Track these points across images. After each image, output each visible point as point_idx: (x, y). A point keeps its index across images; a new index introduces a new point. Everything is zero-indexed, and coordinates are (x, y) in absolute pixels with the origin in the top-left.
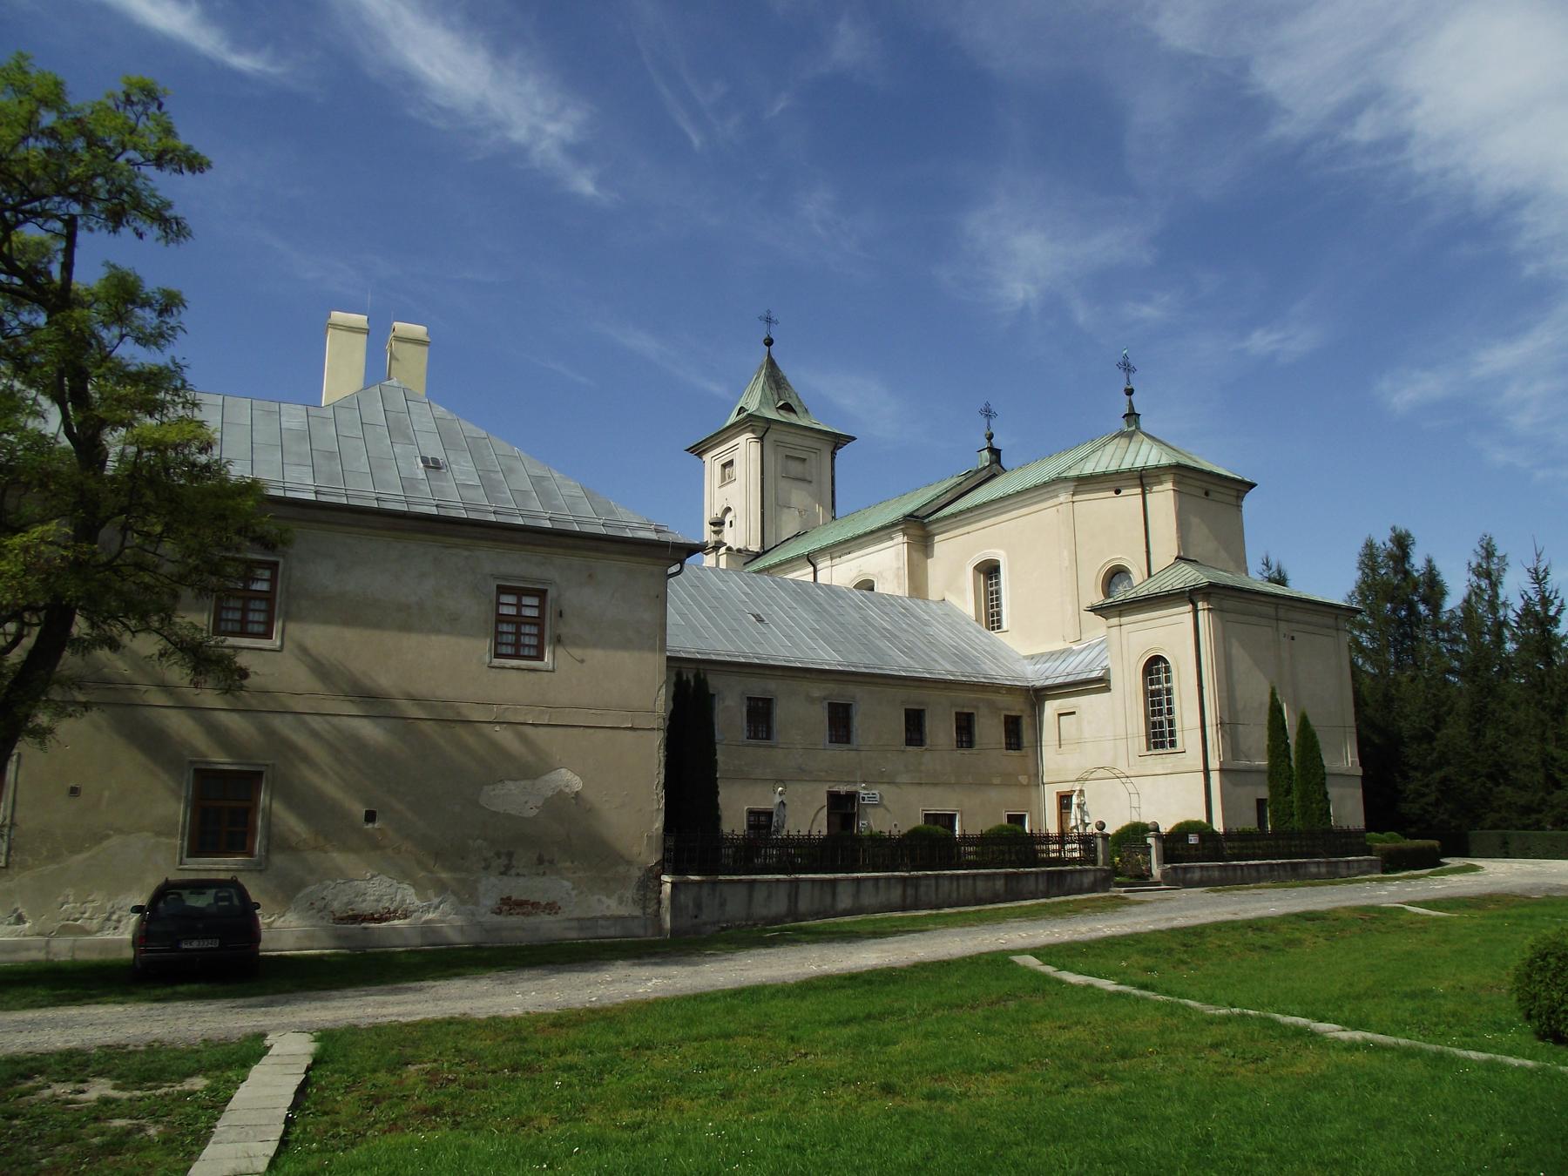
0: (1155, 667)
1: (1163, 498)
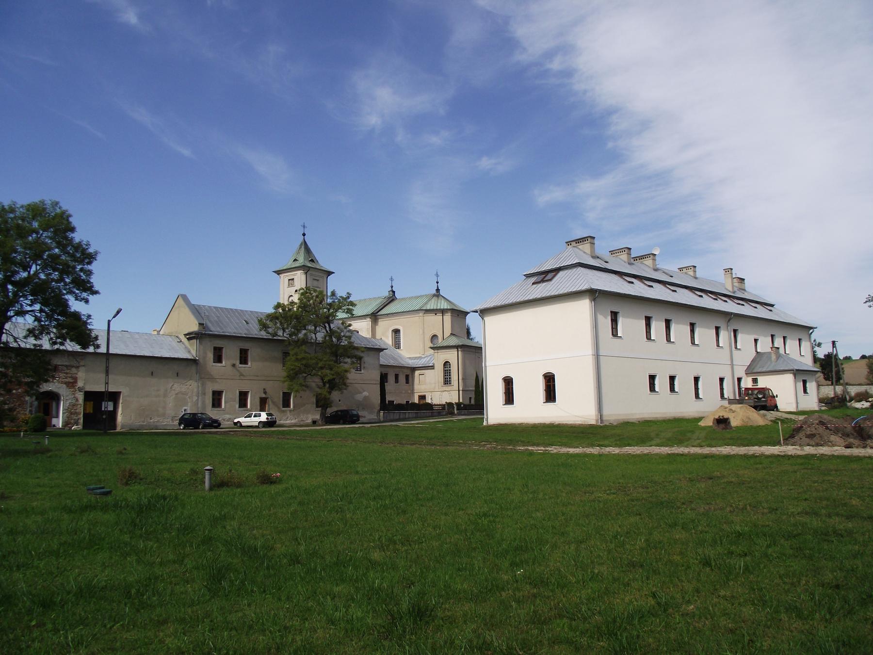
0: (446, 364)
1: (448, 317)
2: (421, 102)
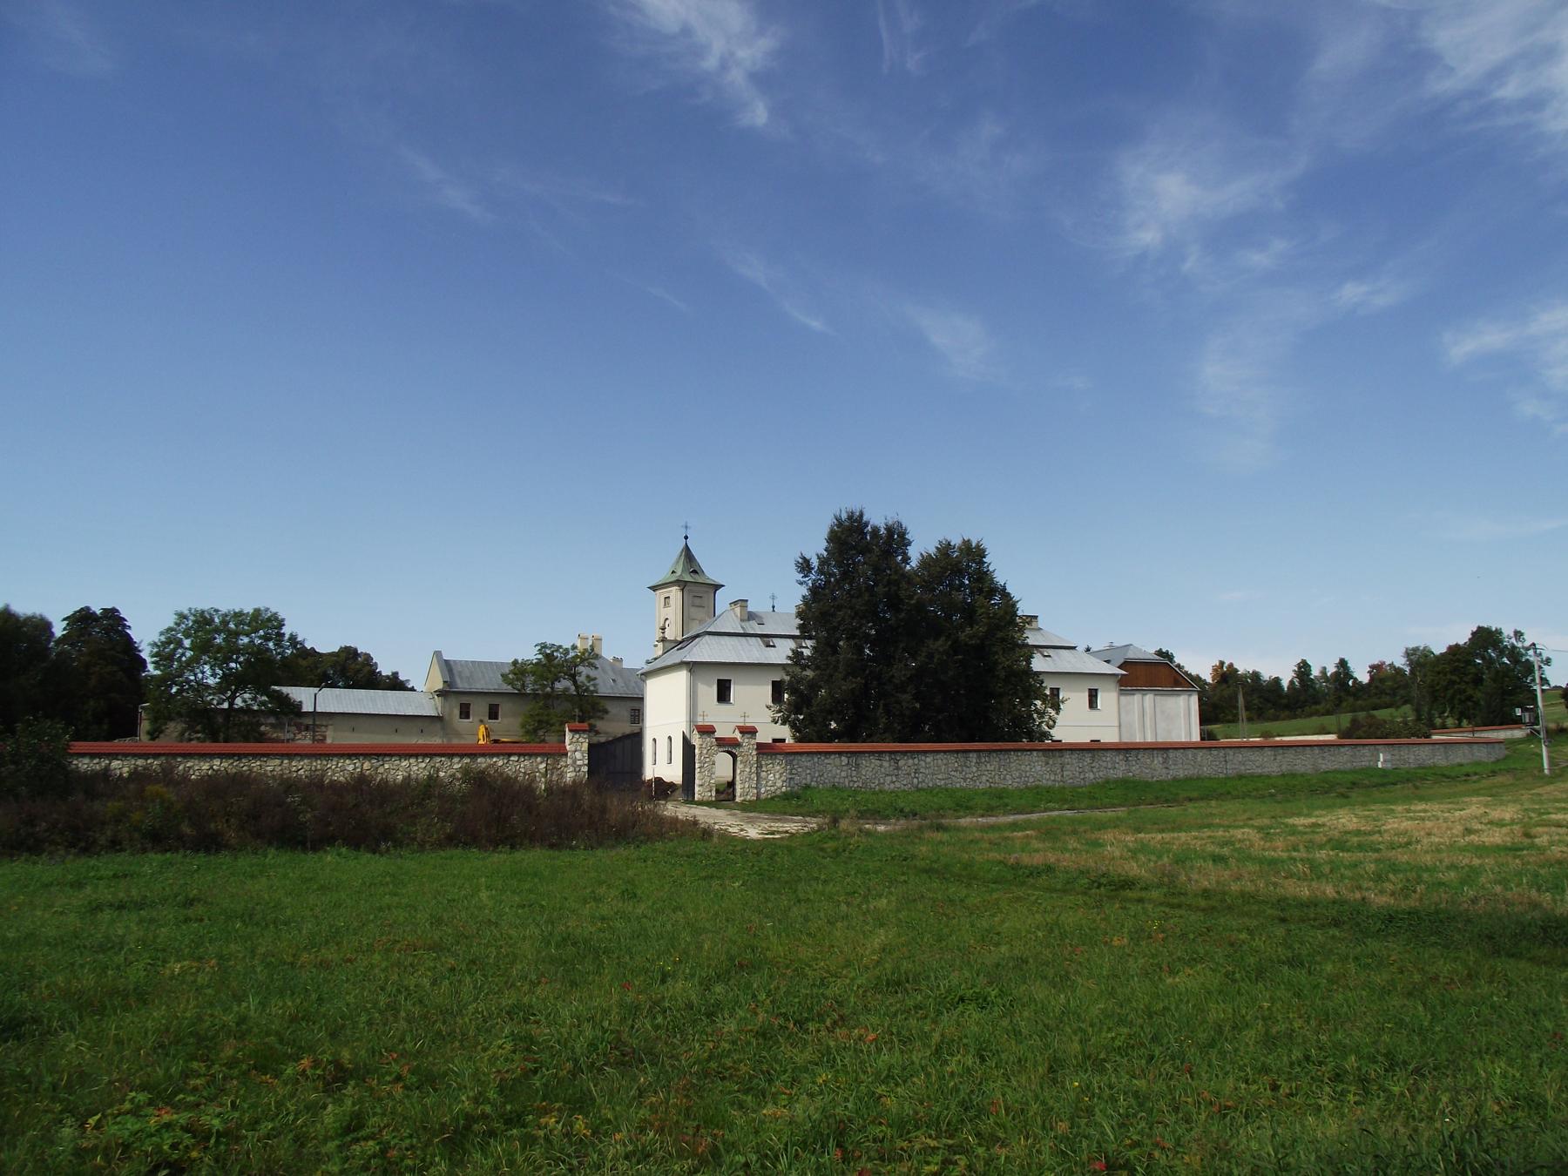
2: (1238, 193)
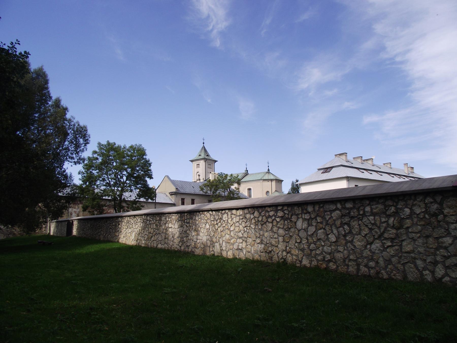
1: (274, 183)
